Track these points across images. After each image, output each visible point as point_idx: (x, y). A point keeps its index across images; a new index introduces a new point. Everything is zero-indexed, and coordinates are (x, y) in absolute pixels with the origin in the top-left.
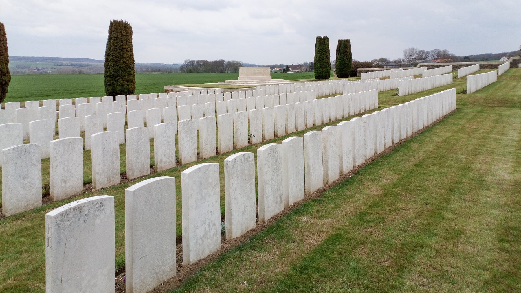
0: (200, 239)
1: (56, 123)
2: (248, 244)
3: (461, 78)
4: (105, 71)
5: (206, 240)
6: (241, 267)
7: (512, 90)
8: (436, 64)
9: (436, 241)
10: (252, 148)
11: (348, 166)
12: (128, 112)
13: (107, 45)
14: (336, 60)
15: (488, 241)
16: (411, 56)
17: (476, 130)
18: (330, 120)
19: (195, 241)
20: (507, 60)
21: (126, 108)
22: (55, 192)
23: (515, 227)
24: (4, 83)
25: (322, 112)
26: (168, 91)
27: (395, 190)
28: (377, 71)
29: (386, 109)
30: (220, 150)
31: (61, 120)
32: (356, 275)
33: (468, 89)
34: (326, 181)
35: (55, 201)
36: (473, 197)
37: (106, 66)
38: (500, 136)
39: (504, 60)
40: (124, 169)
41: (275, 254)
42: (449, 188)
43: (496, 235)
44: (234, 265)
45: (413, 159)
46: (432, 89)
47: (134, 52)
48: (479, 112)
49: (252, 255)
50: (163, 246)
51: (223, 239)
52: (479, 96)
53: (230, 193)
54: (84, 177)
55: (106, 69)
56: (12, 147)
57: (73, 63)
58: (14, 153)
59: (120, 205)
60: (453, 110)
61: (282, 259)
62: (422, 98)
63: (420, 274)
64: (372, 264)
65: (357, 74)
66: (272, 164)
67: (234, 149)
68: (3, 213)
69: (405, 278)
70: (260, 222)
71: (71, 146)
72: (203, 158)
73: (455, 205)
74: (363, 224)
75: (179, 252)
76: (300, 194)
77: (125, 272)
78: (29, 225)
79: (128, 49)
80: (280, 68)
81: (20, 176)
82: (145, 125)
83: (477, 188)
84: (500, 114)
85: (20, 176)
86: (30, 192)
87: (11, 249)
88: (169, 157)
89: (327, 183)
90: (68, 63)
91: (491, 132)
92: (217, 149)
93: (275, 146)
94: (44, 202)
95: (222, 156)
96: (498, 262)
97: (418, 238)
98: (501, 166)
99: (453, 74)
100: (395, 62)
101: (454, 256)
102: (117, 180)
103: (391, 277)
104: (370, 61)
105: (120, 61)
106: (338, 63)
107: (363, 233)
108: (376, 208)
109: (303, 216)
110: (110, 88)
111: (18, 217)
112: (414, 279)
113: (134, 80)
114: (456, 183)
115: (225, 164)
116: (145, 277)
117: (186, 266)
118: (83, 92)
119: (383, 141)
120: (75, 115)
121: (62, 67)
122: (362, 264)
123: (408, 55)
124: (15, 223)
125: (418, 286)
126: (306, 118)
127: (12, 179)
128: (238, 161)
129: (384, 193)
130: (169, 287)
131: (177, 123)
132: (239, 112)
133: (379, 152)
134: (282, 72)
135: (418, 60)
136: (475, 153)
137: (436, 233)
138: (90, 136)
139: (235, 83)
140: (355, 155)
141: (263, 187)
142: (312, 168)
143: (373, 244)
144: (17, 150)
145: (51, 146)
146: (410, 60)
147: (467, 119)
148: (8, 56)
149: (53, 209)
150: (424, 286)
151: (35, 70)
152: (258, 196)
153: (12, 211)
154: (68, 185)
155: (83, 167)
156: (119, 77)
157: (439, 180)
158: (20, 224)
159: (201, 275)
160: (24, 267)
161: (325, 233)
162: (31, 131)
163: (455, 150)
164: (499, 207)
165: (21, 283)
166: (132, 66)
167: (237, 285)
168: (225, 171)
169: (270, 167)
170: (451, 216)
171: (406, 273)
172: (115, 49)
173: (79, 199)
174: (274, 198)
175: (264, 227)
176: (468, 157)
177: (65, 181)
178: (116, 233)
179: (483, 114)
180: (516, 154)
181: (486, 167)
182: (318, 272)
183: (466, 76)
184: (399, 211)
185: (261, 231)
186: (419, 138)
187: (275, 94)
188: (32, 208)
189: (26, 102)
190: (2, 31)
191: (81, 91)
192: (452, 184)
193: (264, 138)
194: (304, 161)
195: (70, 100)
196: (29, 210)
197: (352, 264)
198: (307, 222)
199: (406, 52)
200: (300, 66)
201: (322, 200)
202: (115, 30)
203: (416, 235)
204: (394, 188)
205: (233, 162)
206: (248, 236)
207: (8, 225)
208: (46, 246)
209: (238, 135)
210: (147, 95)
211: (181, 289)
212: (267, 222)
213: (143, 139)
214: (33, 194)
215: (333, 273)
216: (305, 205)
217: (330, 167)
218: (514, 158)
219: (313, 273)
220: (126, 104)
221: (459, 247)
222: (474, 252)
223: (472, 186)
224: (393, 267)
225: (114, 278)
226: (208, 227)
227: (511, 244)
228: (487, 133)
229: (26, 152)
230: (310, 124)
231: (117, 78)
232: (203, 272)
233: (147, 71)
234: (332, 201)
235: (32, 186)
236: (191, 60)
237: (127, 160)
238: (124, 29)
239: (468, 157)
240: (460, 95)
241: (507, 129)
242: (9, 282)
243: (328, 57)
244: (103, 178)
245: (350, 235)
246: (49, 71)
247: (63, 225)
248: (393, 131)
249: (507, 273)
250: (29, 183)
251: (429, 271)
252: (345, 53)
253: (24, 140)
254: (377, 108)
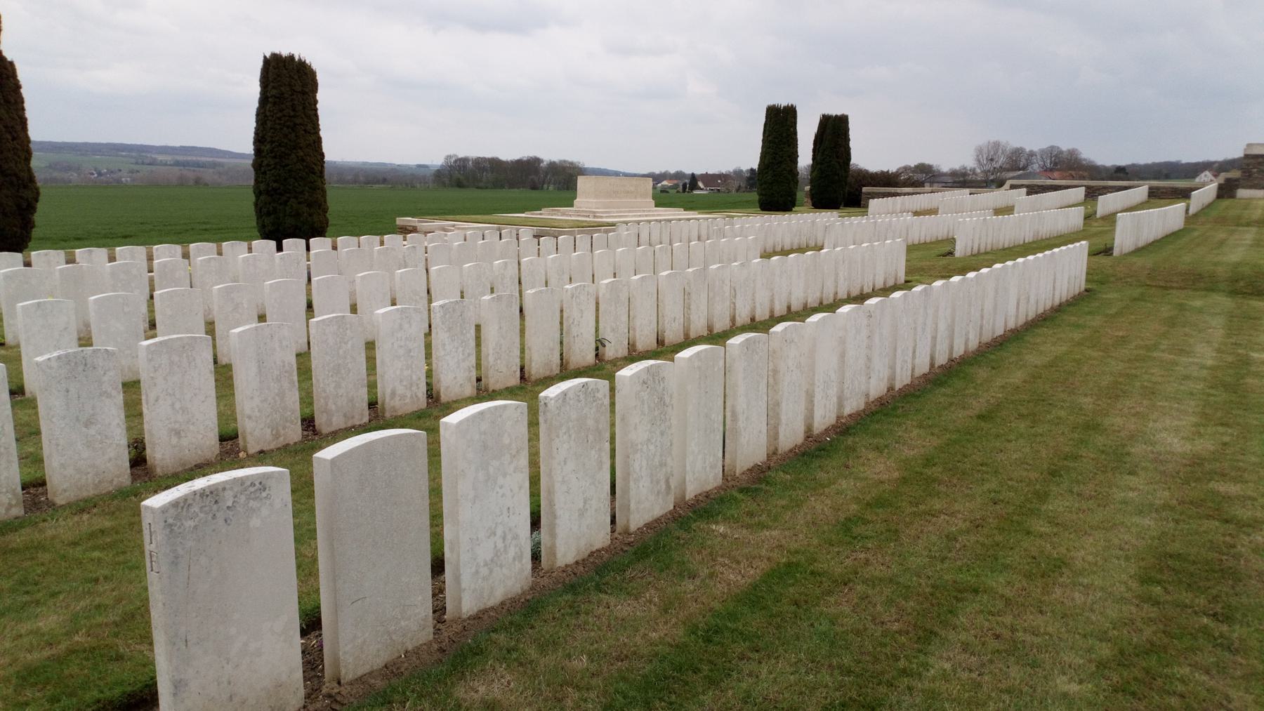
0: (484, 566)
1: (148, 301)
2: (591, 579)
3: (1104, 218)
4: (256, 180)
5: (498, 568)
6: (575, 626)
7: (1215, 252)
8: (1049, 182)
9: (1008, 580)
10: (604, 368)
11: (825, 416)
12: (314, 279)
13: (257, 115)
14: (813, 165)
15: (1119, 582)
16: (992, 160)
17: (1123, 341)
18: (789, 308)
19: (474, 570)
20: (1213, 178)
21: (309, 268)
22: (158, 456)
23: (1180, 554)
24: (24, 205)
25: (772, 290)
26: (405, 231)
27: (928, 472)
28: (909, 194)
29: (924, 286)
30: (529, 373)
31: (160, 294)
32: (827, 648)
33: (1115, 245)
34: (772, 448)
35: (160, 477)
36: (1098, 488)
37: (257, 166)
38: (1175, 355)
39: (1206, 179)
40: (309, 409)
41: (650, 602)
42: (1049, 468)
43: (1137, 569)
44: (559, 622)
45: (974, 403)
46: (1034, 242)
47: (322, 133)
48: (1135, 299)
49: (599, 603)
50: (403, 579)
51: (536, 568)
52: (1139, 261)
53: (551, 470)
54: (219, 426)
55: (256, 173)
56: (55, 354)
57: (180, 158)
58: (61, 367)
59: (303, 489)
60: (1077, 292)
61: (666, 612)
62: (1009, 263)
63: (966, 647)
64: (864, 625)
66: (649, 407)
67: (561, 371)
68: (49, 497)
69: (933, 655)
70: (620, 534)
71: (185, 355)
72: (491, 390)
73: (1055, 505)
74: (850, 543)
75: (438, 592)
76: (711, 476)
77: (320, 628)
78: (108, 524)
79: (309, 127)
80: (676, 182)
81: (78, 419)
82: (354, 309)
83: (1109, 469)
84: (1181, 305)
85: (78, 419)
86: (103, 454)
87: (73, 572)
88: (411, 385)
89: (775, 453)
91: (1155, 347)
92: (522, 369)
93: (659, 366)
94: (134, 477)
95: (533, 386)
96: (1133, 624)
97: (967, 574)
98: (1168, 422)
99: (1086, 208)
100: (954, 174)
101: (1041, 612)
102: (294, 433)
103: (902, 652)
104: (894, 171)
105: (290, 155)
106: (815, 173)
107: (848, 562)
108: (881, 510)
109: (717, 523)
110: (267, 221)
111: (83, 506)
112: (952, 656)
113: (325, 202)
114: (1065, 459)
115: (541, 404)
116: (364, 642)
117: (454, 621)
118: (206, 230)
119: (909, 361)
120: (191, 282)
121: (154, 168)
122: (842, 625)
123: (985, 157)
124: (76, 518)
125: (959, 670)
126: (734, 304)
127: (63, 425)
128: (570, 399)
129: (904, 478)
130: (418, 661)
131: (429, 306)
132: (573, 285)
133: (898, 386)
135: (1008, 170)
136: (1115, 392)
137: (1008, 565)
138: (228, 332)
139: (567, 215)
140: (842, 392)
141: (628, 457)
142: (741, 418)
143: (868, 586)
144: (65, 360)
145: (142, 355)
146: (989, 171)
147: (1107, 315)
148: (28, 141)
149: (156, 492)
150: (971, 671)
151: (93, 174)
152: (615, 477)
153: (67, 494)
154: (185, 442)
155: (215, 404)
156: (288, 195)
157: (1028, 450)
158: (88, 522)
159: (487, 640)
160: (105, 610)
161: (765, 561)
162: (93, 318)
163: (1072, 384)
164: (1151, 512)
165: (102, 642)
166: (320, 168)
167: (567, 662)
168: (541, 420)
169: (645, 415)
170: (1046, 529)
171: (935, 644)
172: (278, 127)
173: (212, 473)
174: (652, 482)
175: (629, 544)
176: (1100, 402)
177: (178, 433)
178: (297, 549)
179: (1143, 303)
180: (1205, 398)
181: (1135, 423)
182: (744, 641)
183: (1115, 214)
184: (933, 516)
185: (621, 553)
186: (993, 357)
187: (661, 243)
188: (111, 489)
189: (77, 251)
190: (11, 79)
191: (201, 227)
192: (1056, 460)
193: (632, 346)
194: (725, 402)
195: (178, 249)
196: (103, 492)
197: (820, 624)
198: (724, 536)
199: (980, 151)
200: (724, 177)
201: (761, 489)
202: (275, 79)
203: (965, 569)
204: (925, 466)
205: (560, 401)
206: (591, 563)
207: (62, 522)
208: (148, 569)
209: (572, 339)
210: (355, 239)
211: (443, 666)
212: (635, 533)
213: (350, 343)
214: (110, 459)
215: (777, 642)
216: (722, 501)
217: (783, 418)
218: (1198, 405)
219: (735, 642)
220: (308, 260)
221: (1056, 593)
222: (1085, 603)
223: (1100, 465)
224: (907, 633)
225: (298, 641)
226: (502, 541)
227: (1166, 589)
228: (1148, 348)
229: (86, 365)
230: (743, 317)
231: (284, 198)
232: (492, 634)
233: (355, 182)
234: (783, 491)
235: (107, 441)
236: (461, 155)
237: (314, 388)
238: (296, 77)
239: (1100, 402)
240: (1096, 259)
241: (1192, 341)
242: (76, 638)
243: (794, 157)
244: (262, 429)
245: (818, 566)
246: (126, 179)
247: (180, 527)
248: (934, 338)
249: (1149, 645)
250: (100, 434)
251: (985, 641)
253: (80, 339)
254: (902, 285)
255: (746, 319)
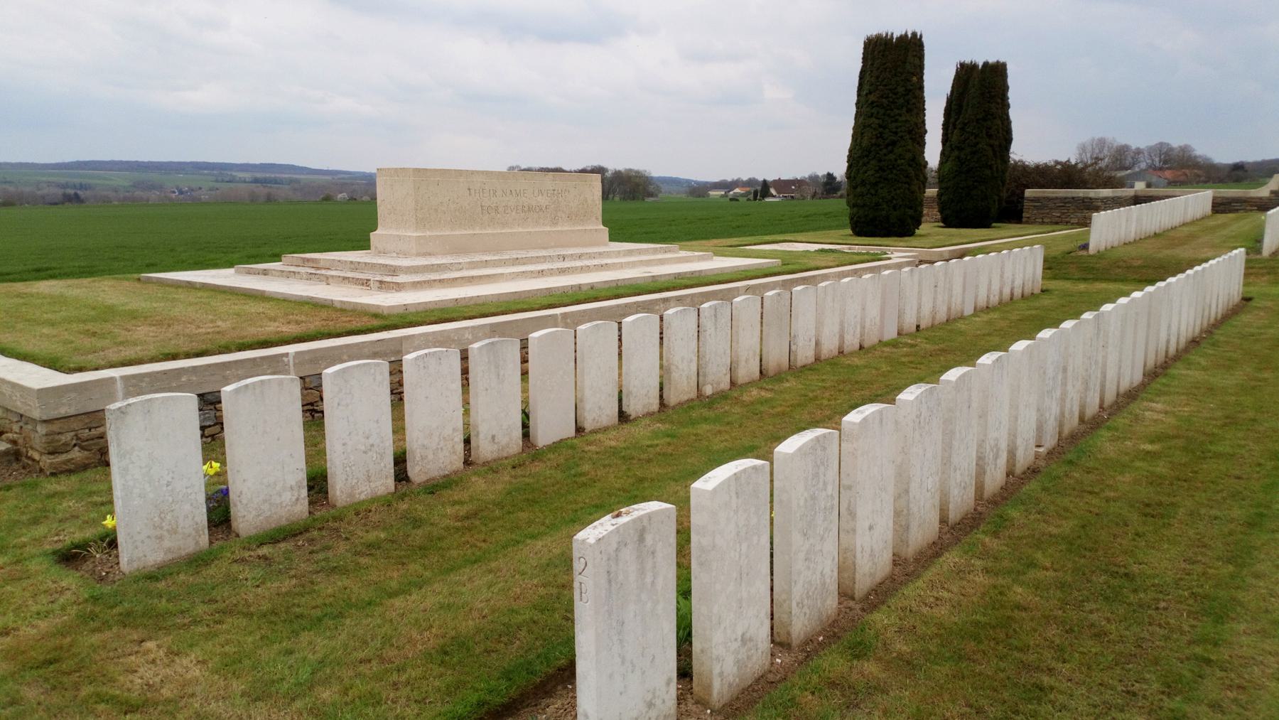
57: (259, 175)
65: (1021, 212)
80: (748, 189)
90: (247, 176)
121: (231, 185)
134: (752, 198)
151: (174, 192)
252: (984, 119)
255: (832, 348)
